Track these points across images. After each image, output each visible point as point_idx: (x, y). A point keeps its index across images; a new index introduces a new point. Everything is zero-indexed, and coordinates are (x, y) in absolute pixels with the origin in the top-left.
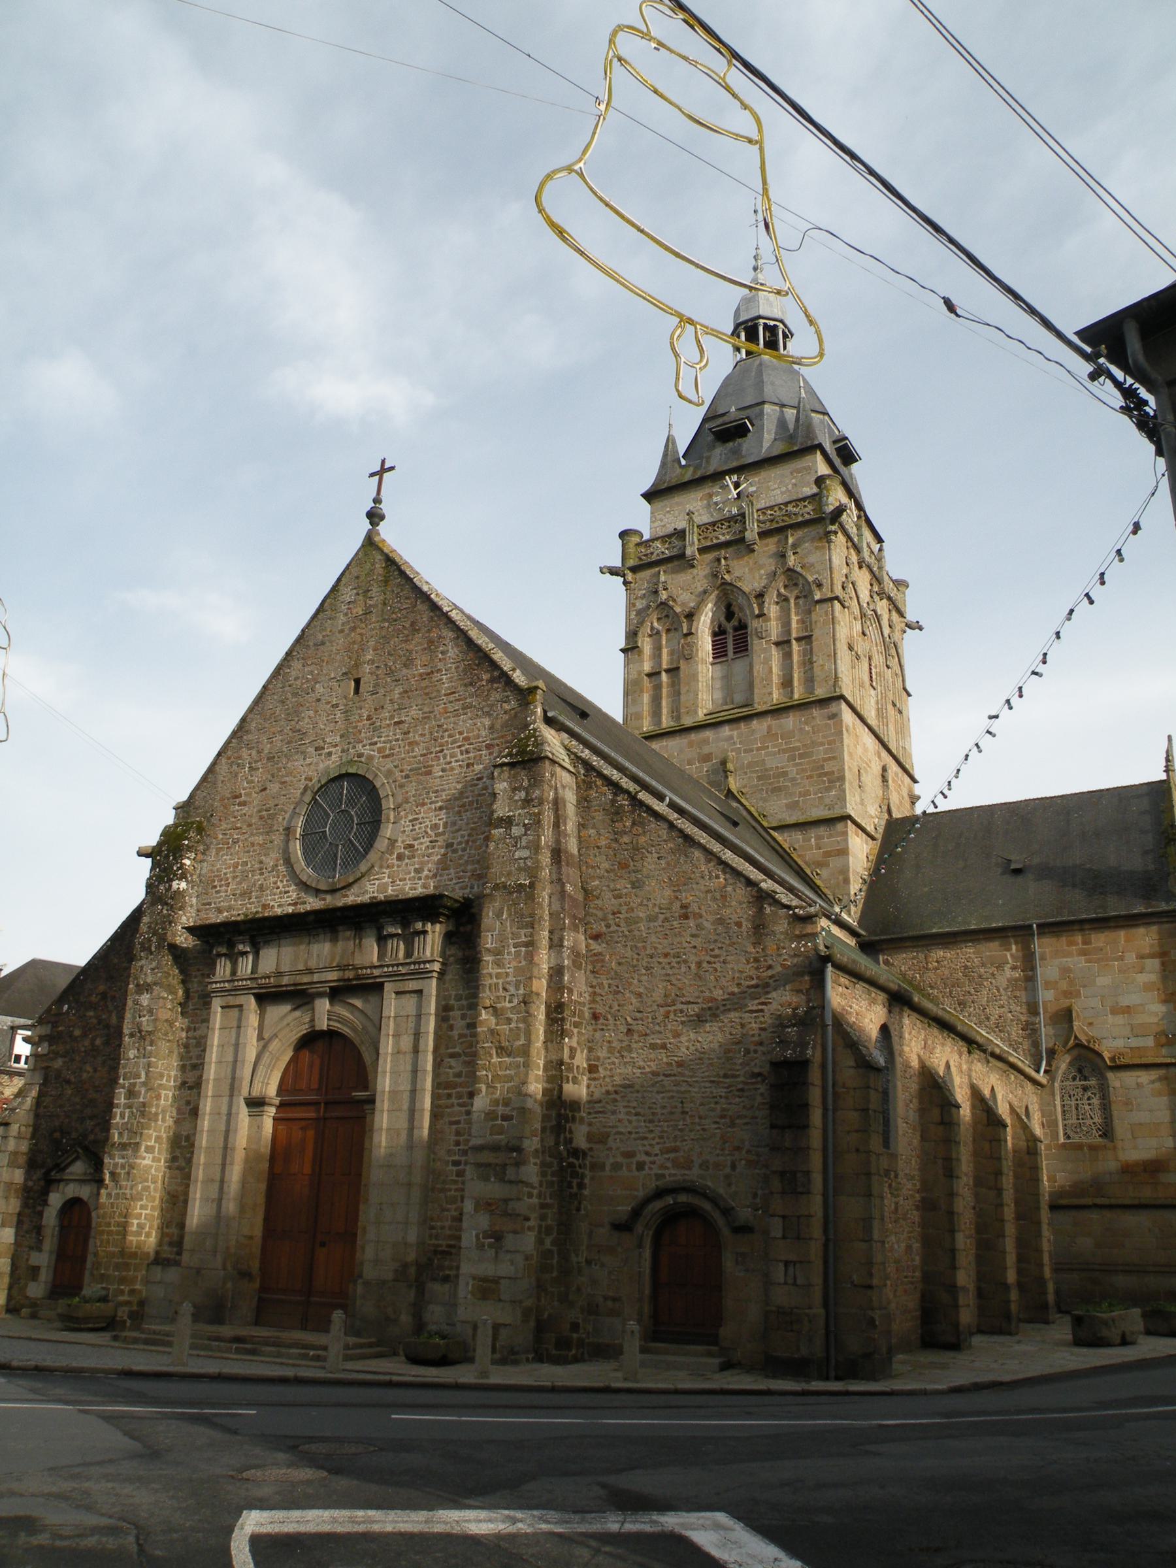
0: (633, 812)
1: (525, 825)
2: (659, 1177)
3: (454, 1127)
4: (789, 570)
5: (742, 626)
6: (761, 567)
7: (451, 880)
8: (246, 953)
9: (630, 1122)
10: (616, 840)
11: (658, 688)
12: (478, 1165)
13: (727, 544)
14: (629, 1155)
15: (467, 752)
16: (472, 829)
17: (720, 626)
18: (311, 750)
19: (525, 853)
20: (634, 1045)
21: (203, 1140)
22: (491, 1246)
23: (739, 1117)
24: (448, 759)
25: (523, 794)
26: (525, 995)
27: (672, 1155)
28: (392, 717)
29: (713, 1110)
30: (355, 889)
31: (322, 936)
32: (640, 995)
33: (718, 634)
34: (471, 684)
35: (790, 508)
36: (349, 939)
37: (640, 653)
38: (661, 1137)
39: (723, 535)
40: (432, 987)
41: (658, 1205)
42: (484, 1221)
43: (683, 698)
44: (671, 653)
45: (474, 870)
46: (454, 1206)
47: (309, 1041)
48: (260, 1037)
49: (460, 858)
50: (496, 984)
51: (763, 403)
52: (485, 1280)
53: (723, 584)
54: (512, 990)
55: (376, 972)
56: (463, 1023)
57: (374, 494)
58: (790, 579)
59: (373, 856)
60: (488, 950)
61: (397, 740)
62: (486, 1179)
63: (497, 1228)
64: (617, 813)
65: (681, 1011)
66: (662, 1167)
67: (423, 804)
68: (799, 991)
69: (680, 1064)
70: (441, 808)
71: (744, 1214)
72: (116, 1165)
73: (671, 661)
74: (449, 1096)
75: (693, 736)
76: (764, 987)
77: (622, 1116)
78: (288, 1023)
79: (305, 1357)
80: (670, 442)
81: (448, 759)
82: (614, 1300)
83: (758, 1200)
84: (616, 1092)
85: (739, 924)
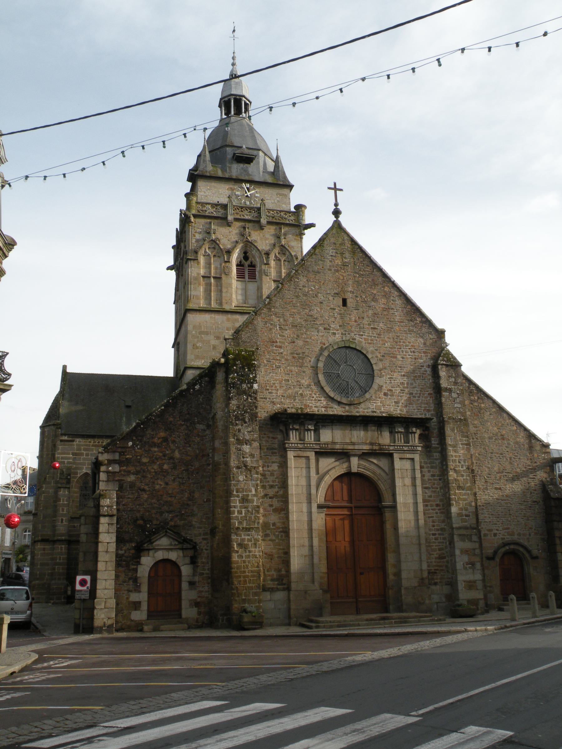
0: (478, 393)
1: (457, 393)
2: (503, 539)
3: (431, 519)
4: (282, 246)
5: (252, 265)
6: (266, 239)
7: (415, 410)
8: (310, 430)
9: (489, 517)
10: (472, 404)
11: (209, 285)
12: (460, 535)
13: (249, 221)
14: (490, 530)
15: (414, 352)
16: (421, 388)
17: (240, 262)
19: (459, 406)
20: (489, 488)
21: (294, 525)
22: (470, 568)
23: (531, 517)
25: (453, 380)
26: (468, 465)
28: (369, 325)
29: (521, 514)
31: (358, 428)
32: (489, 468)
33: (239, 265)
34: (411, 321)
35: (282, 214)
36: (374, 431)
37: (199, 263)
38: (502, 524)
39: (247, 215)
40: (417, 457)
42: (466, 558)
43: (224, 295)
44: (216, 268)
45: (425, 407)
46: (435, 553)
47: (348, 477)
48: (317, 473)
49: (418, 400)
50: (455, 460)
51: (259, 150)
52: (470, 582)
53: (246, 241)
55: (391, 448)
57: (334, 201)
58: (282, 250)
59: (372, 391)
60: (450, 445)
61: (375, 337)
62: (464, 541)
63: (472, 560)
64: (471, 393)
65: (506, 476)
66: (503, 535)
68: (546, 472)
69: (507, 496)
70: (404, 375)
71: (535, 552)
73: (216, 273)
75: (229, 316)
76: (534, 470)
78: (332, 468)
83: (539, 547)
85: (524, 445)
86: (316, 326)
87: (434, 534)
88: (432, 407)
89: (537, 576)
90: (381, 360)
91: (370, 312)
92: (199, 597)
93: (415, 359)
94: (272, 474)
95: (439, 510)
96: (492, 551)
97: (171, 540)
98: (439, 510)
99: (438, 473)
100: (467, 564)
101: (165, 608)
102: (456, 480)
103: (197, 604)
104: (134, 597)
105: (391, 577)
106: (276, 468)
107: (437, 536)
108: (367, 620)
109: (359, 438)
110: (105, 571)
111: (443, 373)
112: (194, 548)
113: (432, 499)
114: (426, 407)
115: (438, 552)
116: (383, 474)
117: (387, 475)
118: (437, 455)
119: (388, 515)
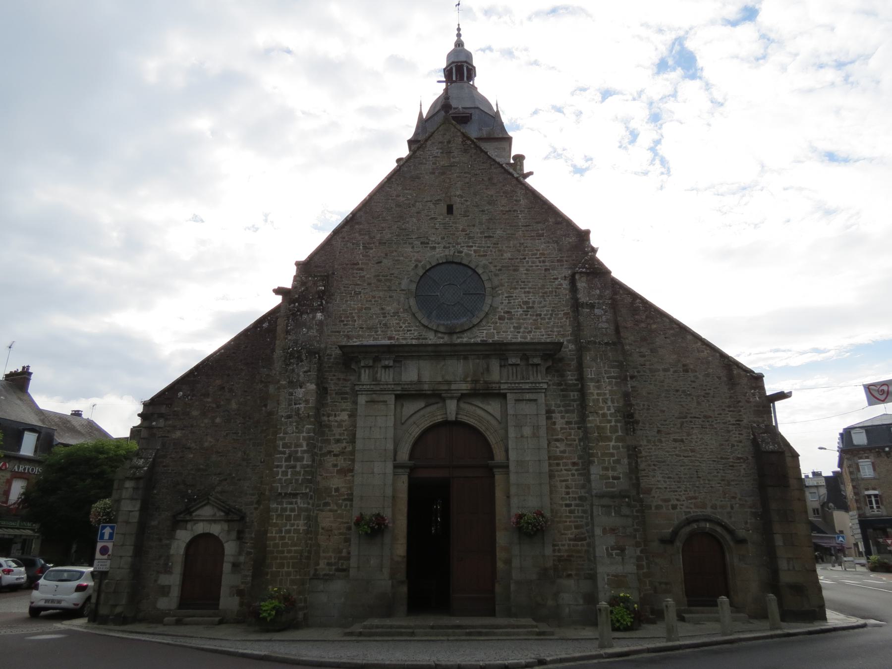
2: (687, 513)
9: (665, 482)
12: (603, 506)
14: (666, 501)
15: (544, 262)
18: (417, 243)
23: (733, 480)
24: (530, 264)
25: (598, 292)
27: (693, 501)
30: (468, 334)
41: (687, 529)
42: (611, 540)
49: (548, 323)
54: (610, 403)
55: (506, 386)
56: (563, 421)
67: (516, 288)
71: (741, 533)
72: (284, 510)
74: (558, 465)
77: (659, 479)
79: (470, 634)
80: (421, 114)
81: (530, 264)
82: (666, 584)
84: (654, 465)
85: (719, 378)
86: (410, 241)
87: (567, 505)
88: (569, 330)
89: (747, 573)
90: (496, 275)
91: (485, 218)
92: (242, 583)
93: (546, 270)
94: (340, 426)
95: (576, 470)
96: (670, 530)
97: (216, 510)
98: (576, 470)
99: (576, 419)
100: (613, 549)
101: (199, 596)
102: (598, 427)
103: (240, 593)
104: (164, 580)
105: (500, 565)
106: (346, 417)
107: (573, 508)
108: (432, 627)
109: (457, 373)
110: (122, 545)
111: (581, 284)
112: (242, 518)
113: (567, 455)
114: (559, 331)
115: (574, 530)
116: (494, 422)
117: (500, 423)
118: (574, 395)
119: (499, 477)
